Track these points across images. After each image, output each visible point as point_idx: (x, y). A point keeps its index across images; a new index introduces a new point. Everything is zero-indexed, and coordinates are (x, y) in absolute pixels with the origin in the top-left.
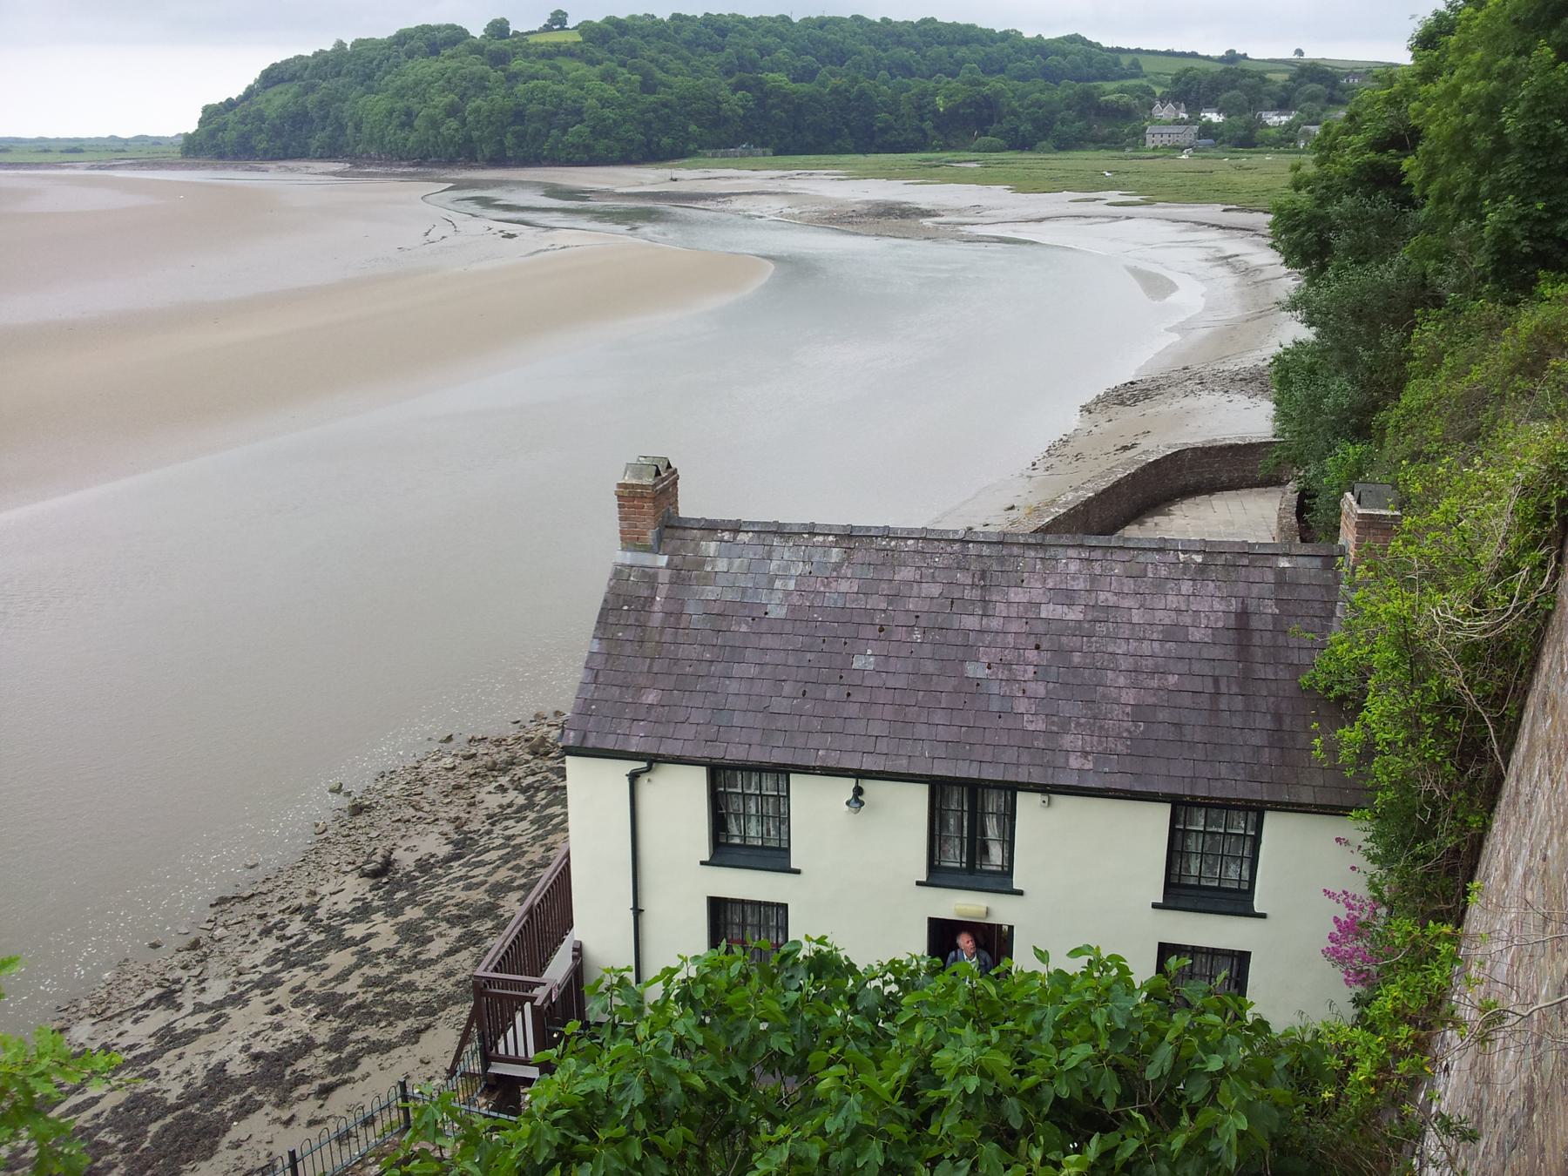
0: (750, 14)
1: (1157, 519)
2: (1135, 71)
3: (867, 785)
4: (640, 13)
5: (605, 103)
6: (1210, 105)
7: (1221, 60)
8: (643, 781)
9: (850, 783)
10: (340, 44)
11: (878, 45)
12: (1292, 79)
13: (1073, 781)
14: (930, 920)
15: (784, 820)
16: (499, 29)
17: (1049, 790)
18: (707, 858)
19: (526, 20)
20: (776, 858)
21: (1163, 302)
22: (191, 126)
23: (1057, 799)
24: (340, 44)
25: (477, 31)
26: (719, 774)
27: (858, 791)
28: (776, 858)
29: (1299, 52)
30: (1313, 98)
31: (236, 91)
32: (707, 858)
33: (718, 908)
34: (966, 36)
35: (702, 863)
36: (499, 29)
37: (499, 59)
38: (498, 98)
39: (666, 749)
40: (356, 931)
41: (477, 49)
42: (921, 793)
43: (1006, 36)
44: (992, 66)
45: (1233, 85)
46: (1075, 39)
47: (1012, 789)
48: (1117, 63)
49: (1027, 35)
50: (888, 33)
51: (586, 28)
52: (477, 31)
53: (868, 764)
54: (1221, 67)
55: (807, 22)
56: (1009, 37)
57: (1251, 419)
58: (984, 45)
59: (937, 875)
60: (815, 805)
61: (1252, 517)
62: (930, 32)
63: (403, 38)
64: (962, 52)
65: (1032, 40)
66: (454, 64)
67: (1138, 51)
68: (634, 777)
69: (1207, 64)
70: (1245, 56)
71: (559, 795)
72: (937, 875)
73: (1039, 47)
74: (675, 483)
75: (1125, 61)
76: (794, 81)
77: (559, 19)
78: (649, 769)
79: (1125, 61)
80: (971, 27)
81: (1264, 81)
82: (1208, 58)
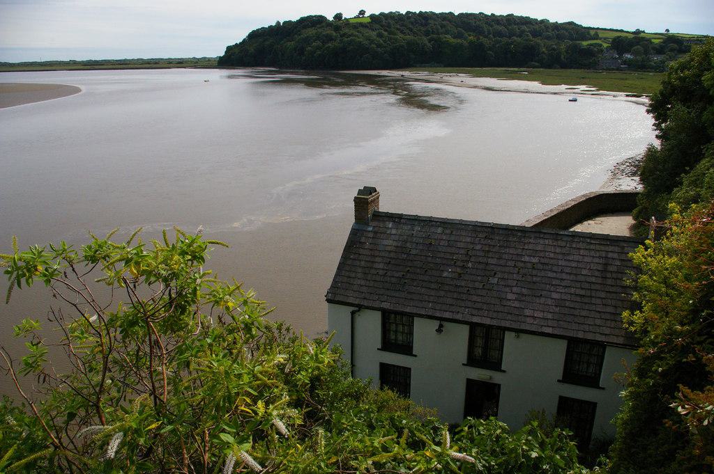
0: (437, 11)
1: (590, 222)
2: (596, 37)
3: (445, 324)
4: (394, 11)
5: (379, 46)
6: (628, 51)
7: (633, 33)
8: (356, 315)
9: (436, 324)
10: (278, 23)
11: (489, 25)
12: (664, 42)
13: (528, 328)
14: (561, 398)
15: (411, 333)
16: (338, 17)
17: (519, 332)
18: (380, 348)
19: (349, 13)
20: (407, 349)
21: (611, 133)
22: (222, 54)
23: (521, 335)
24: (278, 23)
25: (330, 18)
26: (386, 314)
27: (441, 326)
28: (407, 349)
29: (667, 30)
30: (672, 50)
31: (239, 41)
32: (380, 348)
33: (470, 383)
34: (526, 21)
35: (378, 349)
36: (338, 17)
37: (337, 28)
38: (336, 44)
39: (365, 303)
40: (194, 346)
41: (329, 24)
42: (466, 329)
43: (542, 21)
44: (535, 34)
45: (638, 43)
46: (571, 23)
47: (411, 316)
48: (589, 34)
49: (551, 21)
50: (494, 19)
51: (372, 17)
52: (330, 18)
53: (447, 315)
54: (632, 36)
55: (461, 15)
56: (544, 22)
57: (631, 184)
58: (533, 25)
59: (472, 361)
60: (423, 331)
61: (617, 225)
62: (510, 19)
63: (302, 20)
64: (524, 27)
65: (553, 24)
66: (320, 30)
67: (598, 29)
68: (353, 313)
69: (627, 35)
70: (644, 32)
71: (413, 322)
72: (472, 361)
73: (556, 26)
74: (378, 198)
75: (592, 33)
76: (454, 38)
77: (362, 12)
78: (359, 311)
79: (592, 33)
80: (528, 18)
81: (651, 43)
82: (627, 32)
